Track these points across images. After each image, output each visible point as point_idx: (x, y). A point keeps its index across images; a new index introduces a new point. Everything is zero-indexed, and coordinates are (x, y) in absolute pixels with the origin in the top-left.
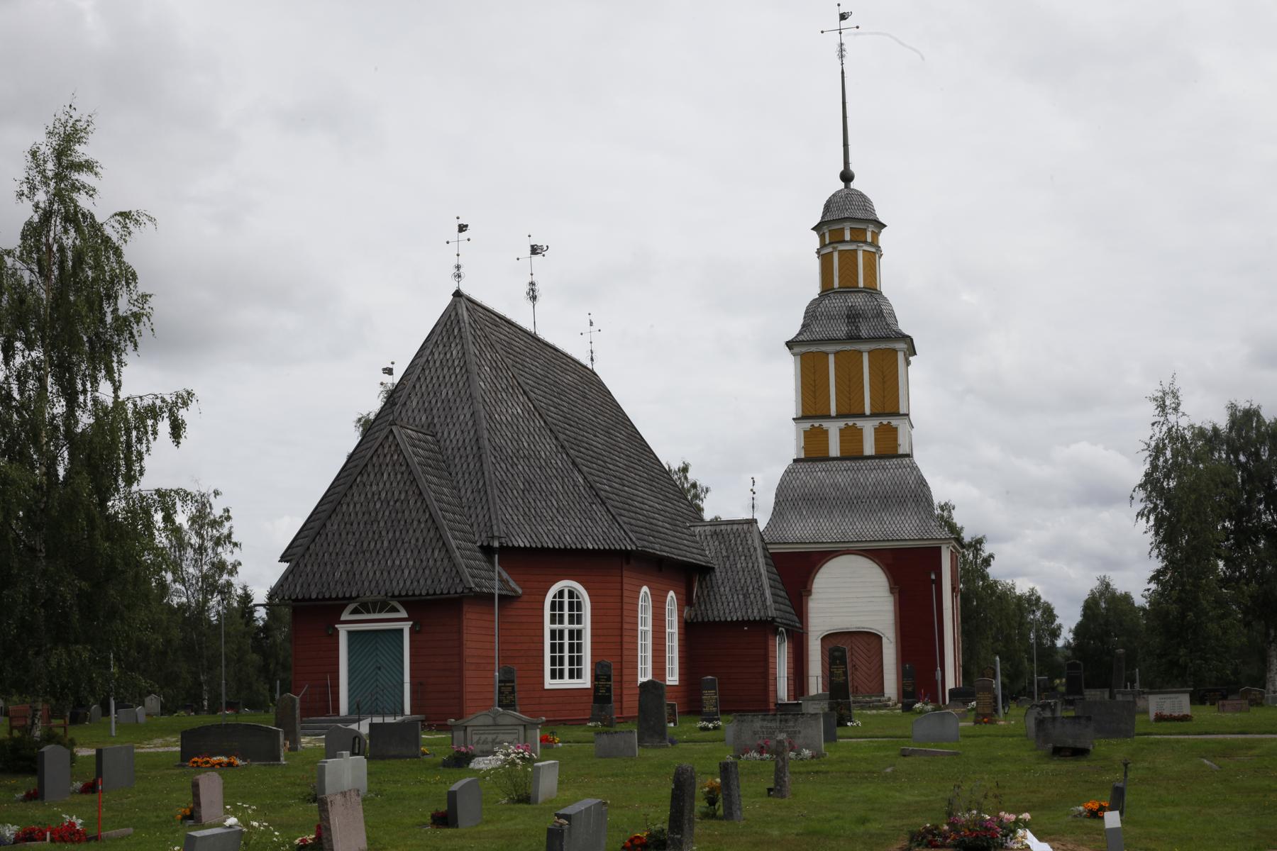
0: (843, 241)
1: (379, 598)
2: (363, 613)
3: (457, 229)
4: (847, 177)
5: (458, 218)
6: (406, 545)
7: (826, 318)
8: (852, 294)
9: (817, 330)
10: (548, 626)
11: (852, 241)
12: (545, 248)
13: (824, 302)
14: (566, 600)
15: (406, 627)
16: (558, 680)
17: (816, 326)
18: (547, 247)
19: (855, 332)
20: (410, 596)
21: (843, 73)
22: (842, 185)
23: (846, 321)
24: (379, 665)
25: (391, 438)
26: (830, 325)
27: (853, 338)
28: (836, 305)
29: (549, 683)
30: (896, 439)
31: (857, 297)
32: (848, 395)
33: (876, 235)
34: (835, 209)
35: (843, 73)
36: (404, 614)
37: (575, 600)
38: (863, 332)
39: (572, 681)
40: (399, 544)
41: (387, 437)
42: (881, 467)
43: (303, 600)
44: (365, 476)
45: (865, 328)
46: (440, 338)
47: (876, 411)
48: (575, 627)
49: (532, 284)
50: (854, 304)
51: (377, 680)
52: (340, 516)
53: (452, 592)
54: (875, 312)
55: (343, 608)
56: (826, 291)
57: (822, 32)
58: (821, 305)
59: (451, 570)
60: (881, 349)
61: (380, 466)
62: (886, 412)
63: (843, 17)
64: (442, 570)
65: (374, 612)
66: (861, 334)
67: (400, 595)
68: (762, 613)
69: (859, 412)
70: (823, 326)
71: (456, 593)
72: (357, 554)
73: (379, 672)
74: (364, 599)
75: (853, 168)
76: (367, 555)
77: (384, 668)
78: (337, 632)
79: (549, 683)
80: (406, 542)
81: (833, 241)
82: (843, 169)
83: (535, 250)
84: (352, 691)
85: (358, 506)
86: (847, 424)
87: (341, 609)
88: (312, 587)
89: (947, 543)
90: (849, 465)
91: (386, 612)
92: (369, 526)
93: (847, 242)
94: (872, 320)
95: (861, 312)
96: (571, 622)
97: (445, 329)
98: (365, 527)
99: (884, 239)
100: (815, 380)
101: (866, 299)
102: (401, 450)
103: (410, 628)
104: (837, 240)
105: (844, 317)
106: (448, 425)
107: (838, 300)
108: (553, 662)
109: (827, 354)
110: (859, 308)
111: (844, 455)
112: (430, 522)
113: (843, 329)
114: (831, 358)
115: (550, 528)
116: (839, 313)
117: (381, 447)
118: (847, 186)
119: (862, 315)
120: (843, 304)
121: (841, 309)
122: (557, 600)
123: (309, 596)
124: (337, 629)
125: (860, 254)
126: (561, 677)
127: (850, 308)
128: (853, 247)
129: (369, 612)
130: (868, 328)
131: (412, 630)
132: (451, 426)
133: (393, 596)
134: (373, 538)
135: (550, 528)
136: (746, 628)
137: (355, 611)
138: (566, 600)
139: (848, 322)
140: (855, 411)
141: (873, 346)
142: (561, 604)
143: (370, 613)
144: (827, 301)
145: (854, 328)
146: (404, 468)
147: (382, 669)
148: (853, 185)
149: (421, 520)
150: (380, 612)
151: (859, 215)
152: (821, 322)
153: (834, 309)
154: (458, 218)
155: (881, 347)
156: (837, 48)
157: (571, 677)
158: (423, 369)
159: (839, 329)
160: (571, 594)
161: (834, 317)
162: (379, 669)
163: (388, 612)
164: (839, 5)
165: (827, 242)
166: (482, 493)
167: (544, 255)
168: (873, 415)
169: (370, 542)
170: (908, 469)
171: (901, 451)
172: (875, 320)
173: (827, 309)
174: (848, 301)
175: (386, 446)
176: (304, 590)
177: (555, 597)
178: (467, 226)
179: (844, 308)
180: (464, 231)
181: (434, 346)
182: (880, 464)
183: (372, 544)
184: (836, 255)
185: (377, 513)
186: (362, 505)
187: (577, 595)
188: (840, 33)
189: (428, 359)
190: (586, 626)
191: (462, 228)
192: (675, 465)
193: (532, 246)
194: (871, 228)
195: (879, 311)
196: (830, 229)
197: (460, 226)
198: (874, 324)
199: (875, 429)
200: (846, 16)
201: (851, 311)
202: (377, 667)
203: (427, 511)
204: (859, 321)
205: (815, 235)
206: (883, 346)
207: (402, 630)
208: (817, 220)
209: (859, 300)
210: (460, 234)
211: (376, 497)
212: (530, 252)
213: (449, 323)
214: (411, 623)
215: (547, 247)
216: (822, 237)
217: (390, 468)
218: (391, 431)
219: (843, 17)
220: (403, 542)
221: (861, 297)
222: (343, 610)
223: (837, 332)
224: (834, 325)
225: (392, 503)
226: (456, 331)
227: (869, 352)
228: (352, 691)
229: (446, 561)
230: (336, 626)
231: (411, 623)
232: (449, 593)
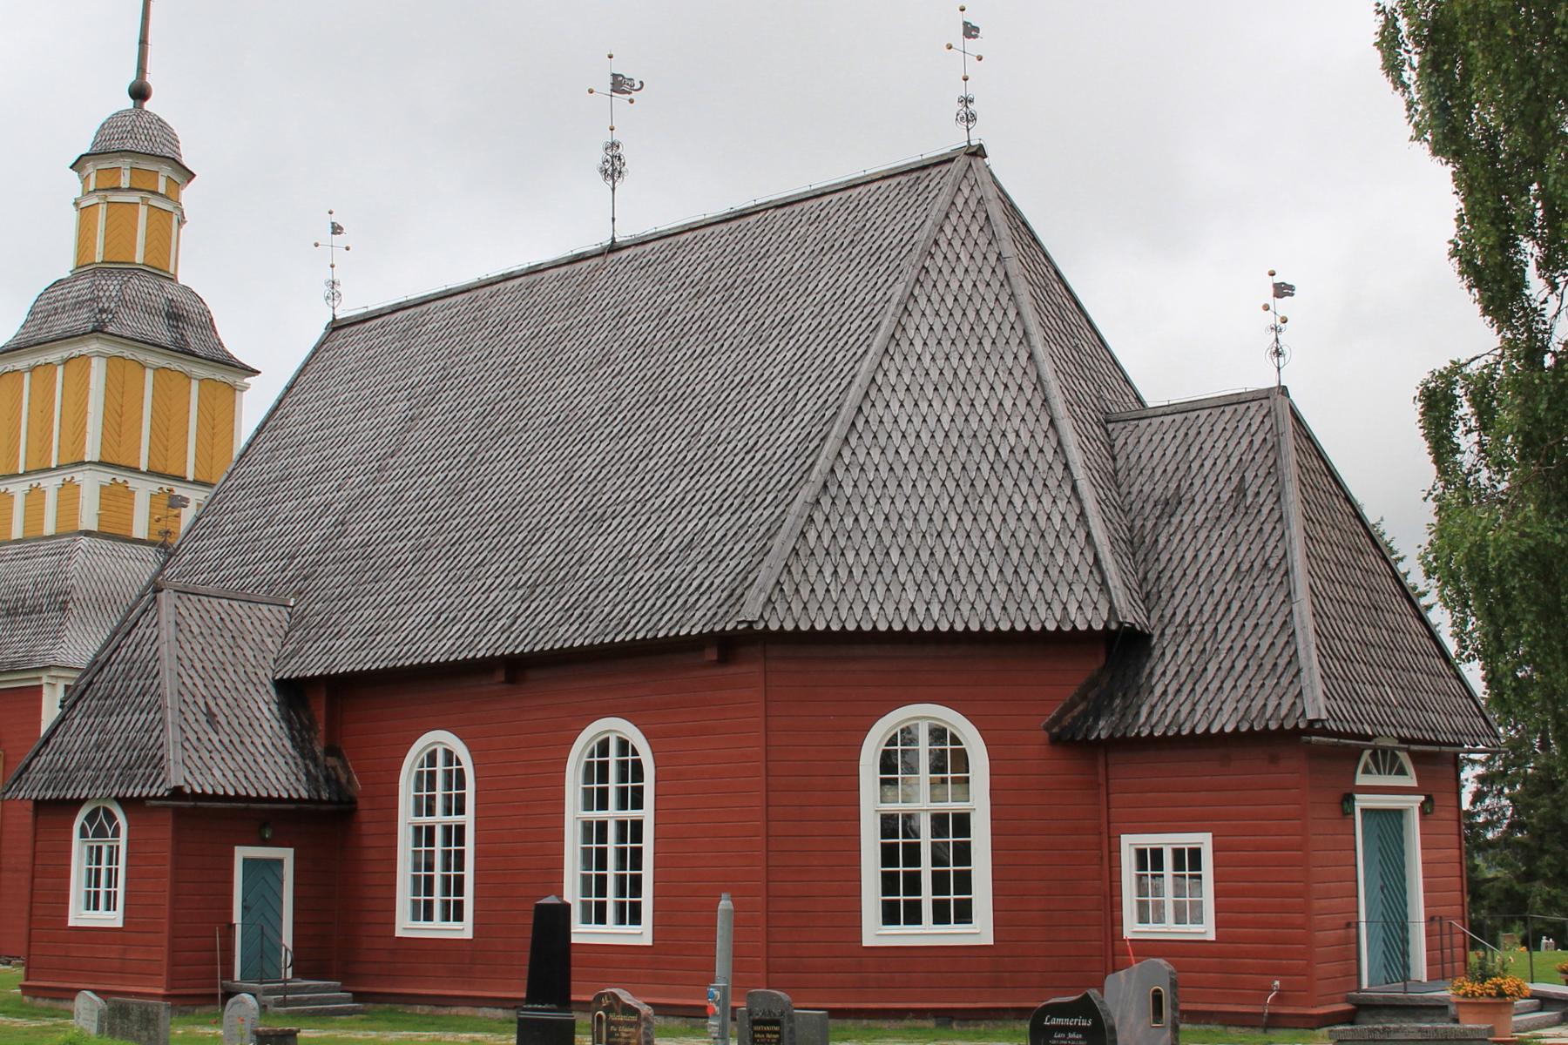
0: (118, 189)
4: (140, 93)
10: (647, 814)
12: (637, 86)
14: (613, 758)
15: (1413, 803)
16: (593, 925)
18: (641, 83)
22: (129, 103)
29: (875, 932)
33: (175, 187)
37: (630, 758)
39: (446, 925)
47: (201, 478)
48: (425, 820)
49: (614, 145)
60: (123, 357)
69: (133, 465)
75: (149, 79)
79: (875, 932)
83: (619, 84)
86: (114, 479)
95: (185, 314)
96: (622, 805)
100: (122, 406)
104: (108, 186)
108: (637, 882)
109: (189, 377)
122: (596, 759)
125: (143, 210)
126: (914, 916)
128: (134, 198)
138: (613, 758)
140: (171, 470)
142: (604, 767)
148: (147, 105)
157: (941, 916)
160: (938, 734)
167: (631, 101)
177: (892, 741)
184: (102, 210)
187: (457, 758)
190: (574, 813)
193: (615, 76)
194: (165, 171)
205: (73, 180)
212: (610, 87)
215: (641, 83)
216: (85, 180)
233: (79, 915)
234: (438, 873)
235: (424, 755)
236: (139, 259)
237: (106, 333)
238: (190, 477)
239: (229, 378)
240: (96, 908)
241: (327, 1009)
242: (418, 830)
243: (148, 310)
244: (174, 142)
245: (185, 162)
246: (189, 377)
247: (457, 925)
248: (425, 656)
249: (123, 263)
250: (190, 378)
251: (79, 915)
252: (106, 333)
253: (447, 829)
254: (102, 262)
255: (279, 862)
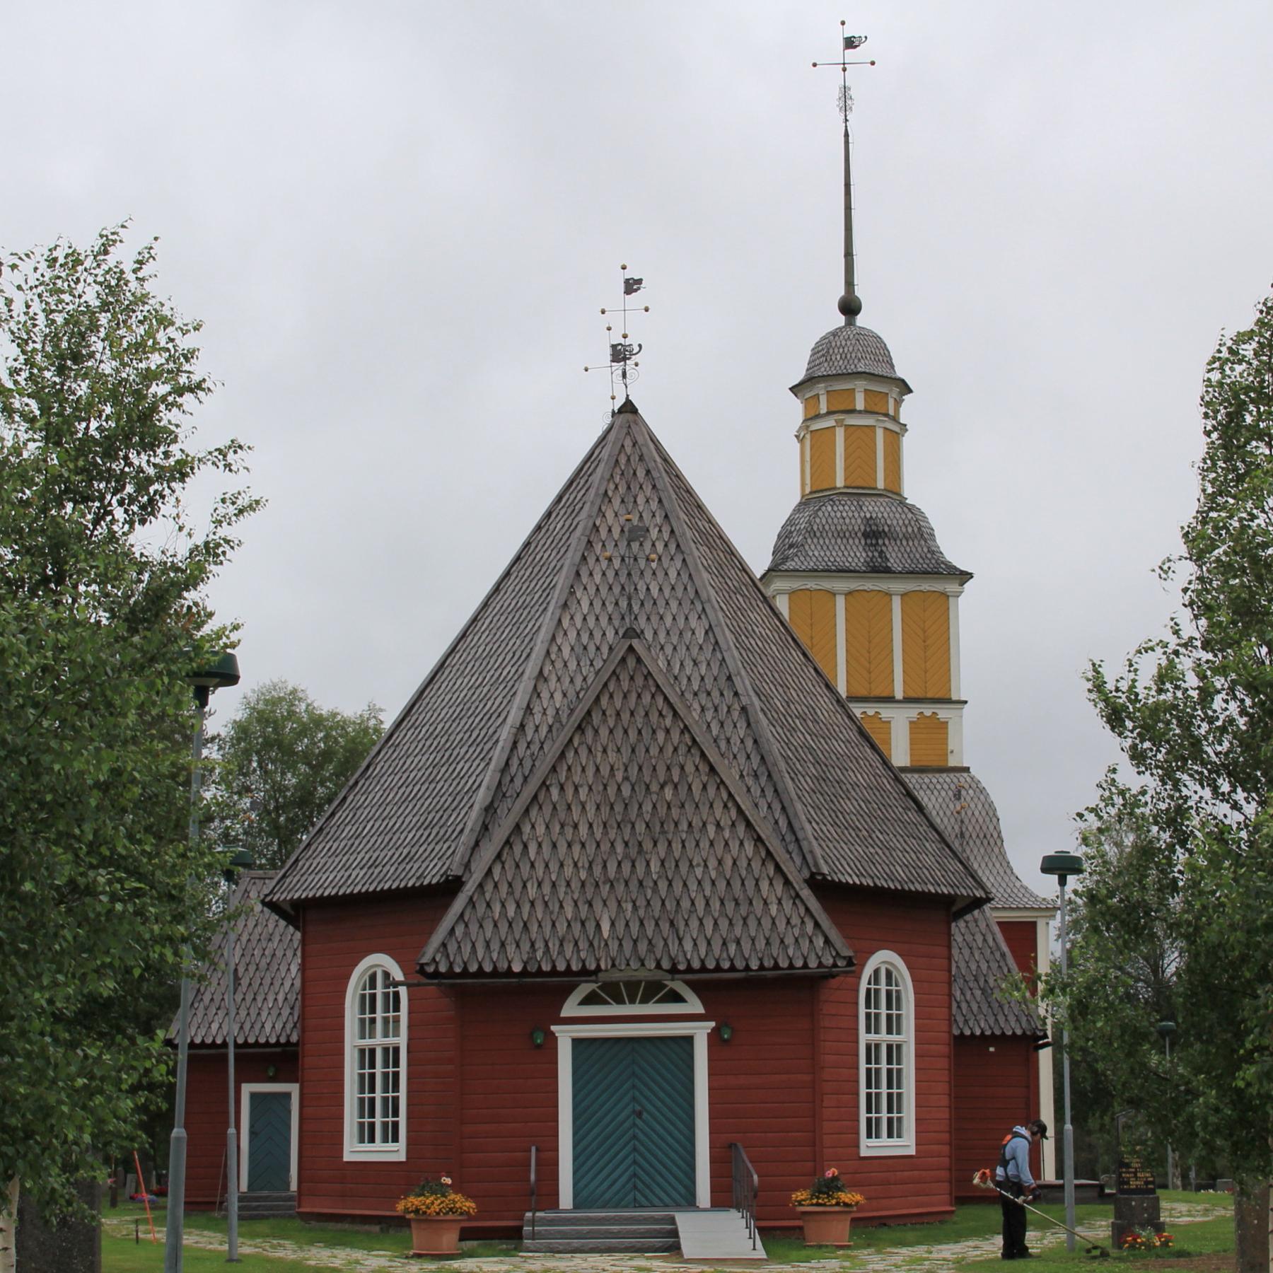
0: (852, 411)
1: (642, 975)
2: (609, 1003)
3: (622, 288)
4: (850, 307)
5: (624, 268)
6: (699, 871)
7: (830, 535)
8: (869, 499)
9: (816, 553)
11: (867, 412)
12: (636, 349)
13: (824, 508)
15: (701, 1033)
16: (390, 1144)
17: (813, 547)
18: (640, 346)
19: (879, 560)
20: (799, 968)
21: (847, 135)
22: (840, 320)
23: (863, 542)
24: (638, 1108)
25: (631, 662)
26: (837, 548)
27: (879, 569)
28: (844, 514)
30: (945, 741)
31: (878, 504)
32: (868, 665)
34: (838, 357)
35: (847, 135)
36: (694, 1005)
38: (892, 561)
40: (684, 868)
41: (623, 660)
42: (924, 787)
43: (495, 973)
44: (589, 733)
45: (894, 555)
46: (612, 486)
47: (912, 694)
48: (367, 1042)
50: (874, 516)
51: (635, 1137)
52: (547, 810)
53: (813, 964)
54: (910, 530)
55: (567, 991)
56: (815, 492)
57: (815, 65)
58: (820, 514)
59: (803, 922)
60: (921, 591)
61: (618, 714)
62: (929, 695)
63: (850, 43)
64: (784, 921)
65: (632, 1001)
66: (889, 564)
67: (689, 970)
68: (1024, 1025)
69: (885, 694)
70: (825, 548)
71: (820, 965)
72: (597, 885)
73: (638, 1122)
74: (615, 976)
75: (859, 292)
76: (620, 888)
77: (648, 1112)
78: (552, 1039)
80: (698, 865)
81: (834, 409)
82: (842, 293)
84: (582, 1159)
85: (583, 792)
86: (921, 713)
87: (564, 992)
88: (511, 949)
89: (1046, 917)
90: (927, 780)
91: (657, 1002)
92: (612, 833)
93: (860, 412)
94: (904, 542)
95: (886, 529)
97: (618, 471)
98: (605, 833)
99: (909, 410)
100: (812, 638)
101: (894, 509)
102: (658, 686)
103: (708, 1034)
104: (842, 408)
105: (859, 535)
106: (662, 648)
107: (847, 508)
109: (889, 595)
110: (883, 520)
111: (915, 764)
112: (741, 828)
113: (858, 554)
114: (896, 603)
115: (872, 850)
116: (850, 528)
117: (614, 678)
118: (850, 322)
119: (889, 535)
120: (856, 515)
121: (853, 521)
123: (506, 966)
124: (553, 1034)
125: (880, 434)
127: (868, 520)
128: (830, 422)
129: (620, 1001)
130: (900, 555)
131: (714, 1038)
132: (669, 650)
133: (674, 970)
134: (626, 856)
135: (872, 850)
136: (992, 1049)
137: (589, 1000)
139: (866, 543)
140: (877, 692)
141: (911, 585)
143: (625, 1003)
144: (829, 508)
145: (876, 554)
146: (668, 721)
147: (645, 1115)
148: (861, 320)
149: (722, 824)
150: (645, 1000)
151: (878, 371)
152: (821, 542)
153: (841, 521)
154: (624, 268)
155: (922, 588)
156: (836, 93)
158: (589, 542)
159: (852, 554)
160: (889, 974)
161: (841, 535)
162: (639, 1115)
163: (660, 1001)
164: (843, 23)
165: (823, 410)
166: (763, 779)
168: (908, 700)
169: (605, 863)
170: (971, 792)
171: (952, 762)
172: (911, 543)
173: (830, 521)
174: (865, 509)
175: (624, 677)
176: (495, 956)
178: (639, 281)
179: (859, 521)
180: (636, 290)
181: (602, 501)
182: (921, 781)
183: (626, 868)
184: (840, 434)
185: (626, 805)
186: (590, 789)
188: (844, 70)
189: (594, 524)
191: (632, 286)
192: (950, 748)
195: (916, 530)
196: (830, 389)
197: (627, 281)
198: (908, 550)
199: (911, 722)
200: (856, 43)
201: (870, 526)
202: (634, 1112)
203: (730, 805)
204: (884, 544)
206: (926, 586)
207: (689, 1040)
208: (799, 375)
209: (882, 509)
210: (627, 297)
211: (619, 776)
212: (609, 358)
213: (623, 460)
214: (713, 1024)
215: (640, 346)
216: (810, 403)
217: (639, 720)
218: (631, 649)
219: (850, 43)
220: (691, 865)
221: (884, 504)
222: (564, 1002)
223: (850, 560)
224: (843, 548)
225: (654, 787)
226: (641, 473)
227: (903, 595)
228: (582, 1159)
229: (788, 905)
230: (553, 1028)
231: (713, 1024)
232: (805, 966)
233: (354, 1150)
234: (378, 1095)
235: (367, 977)
236: (840, 482)
237: (780, 570)
238: (899, 695)
239: (938, 586)
240: (372, 1140)
241: (652, 1217)
242: (362, 1051)
243: (841, 535)
244: (885, 357)
245: (900, 372)
246: (889, 595)
247: (391, 1146)
248: (433, 876)
249: (863, 488)
250: (891, 595)
251: (354, 1150)
252: (780, 570)
253: (386, 1050)
254: (846, 487)
255: (287, 1096)
